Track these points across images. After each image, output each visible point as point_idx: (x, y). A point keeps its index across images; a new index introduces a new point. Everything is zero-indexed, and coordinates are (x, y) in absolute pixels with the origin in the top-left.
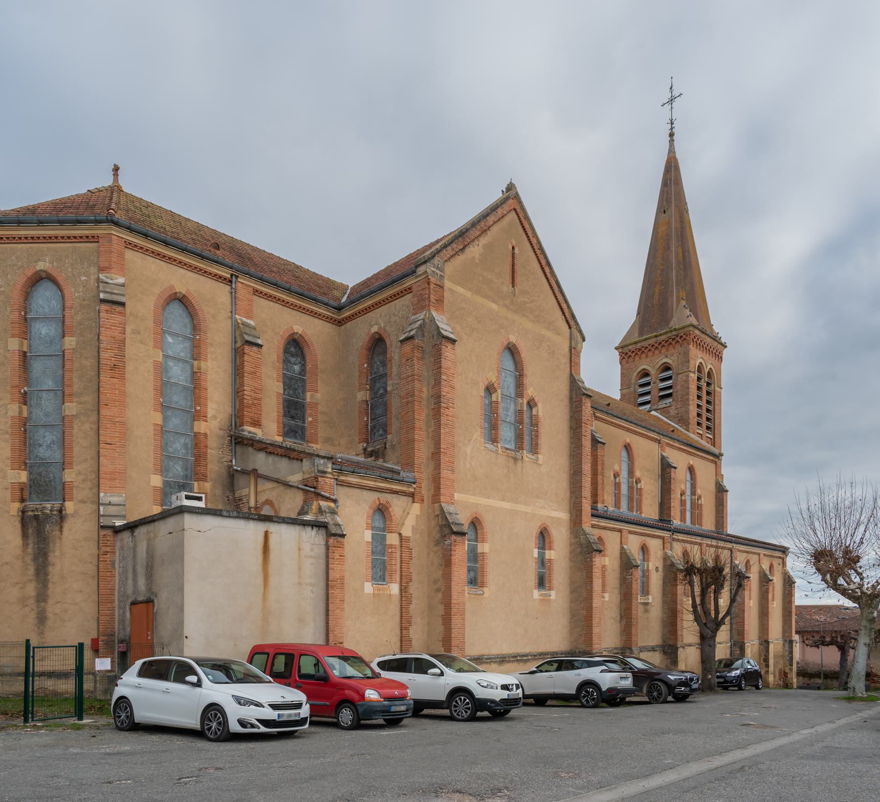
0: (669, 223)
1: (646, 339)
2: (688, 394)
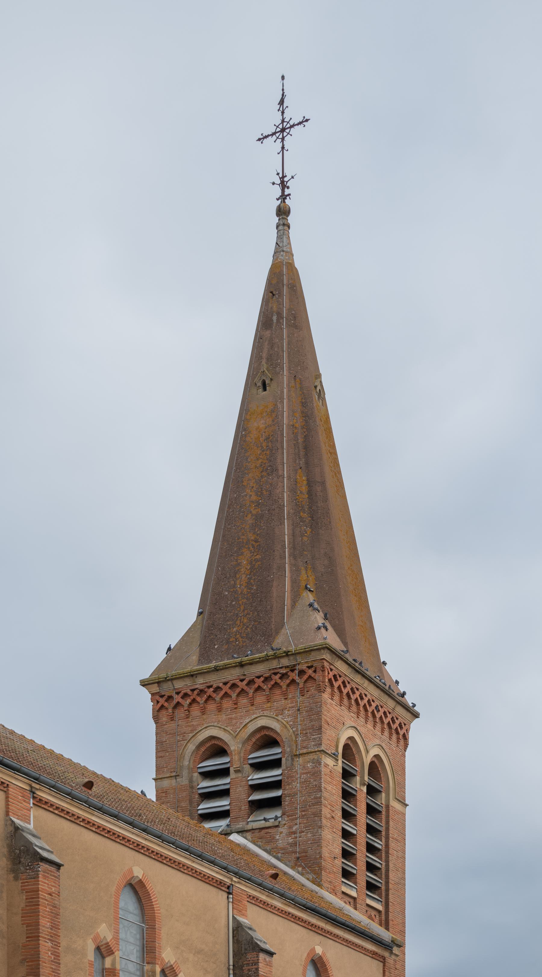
0: (274, 413)
1: (216, 669)
2: (318, 802)
